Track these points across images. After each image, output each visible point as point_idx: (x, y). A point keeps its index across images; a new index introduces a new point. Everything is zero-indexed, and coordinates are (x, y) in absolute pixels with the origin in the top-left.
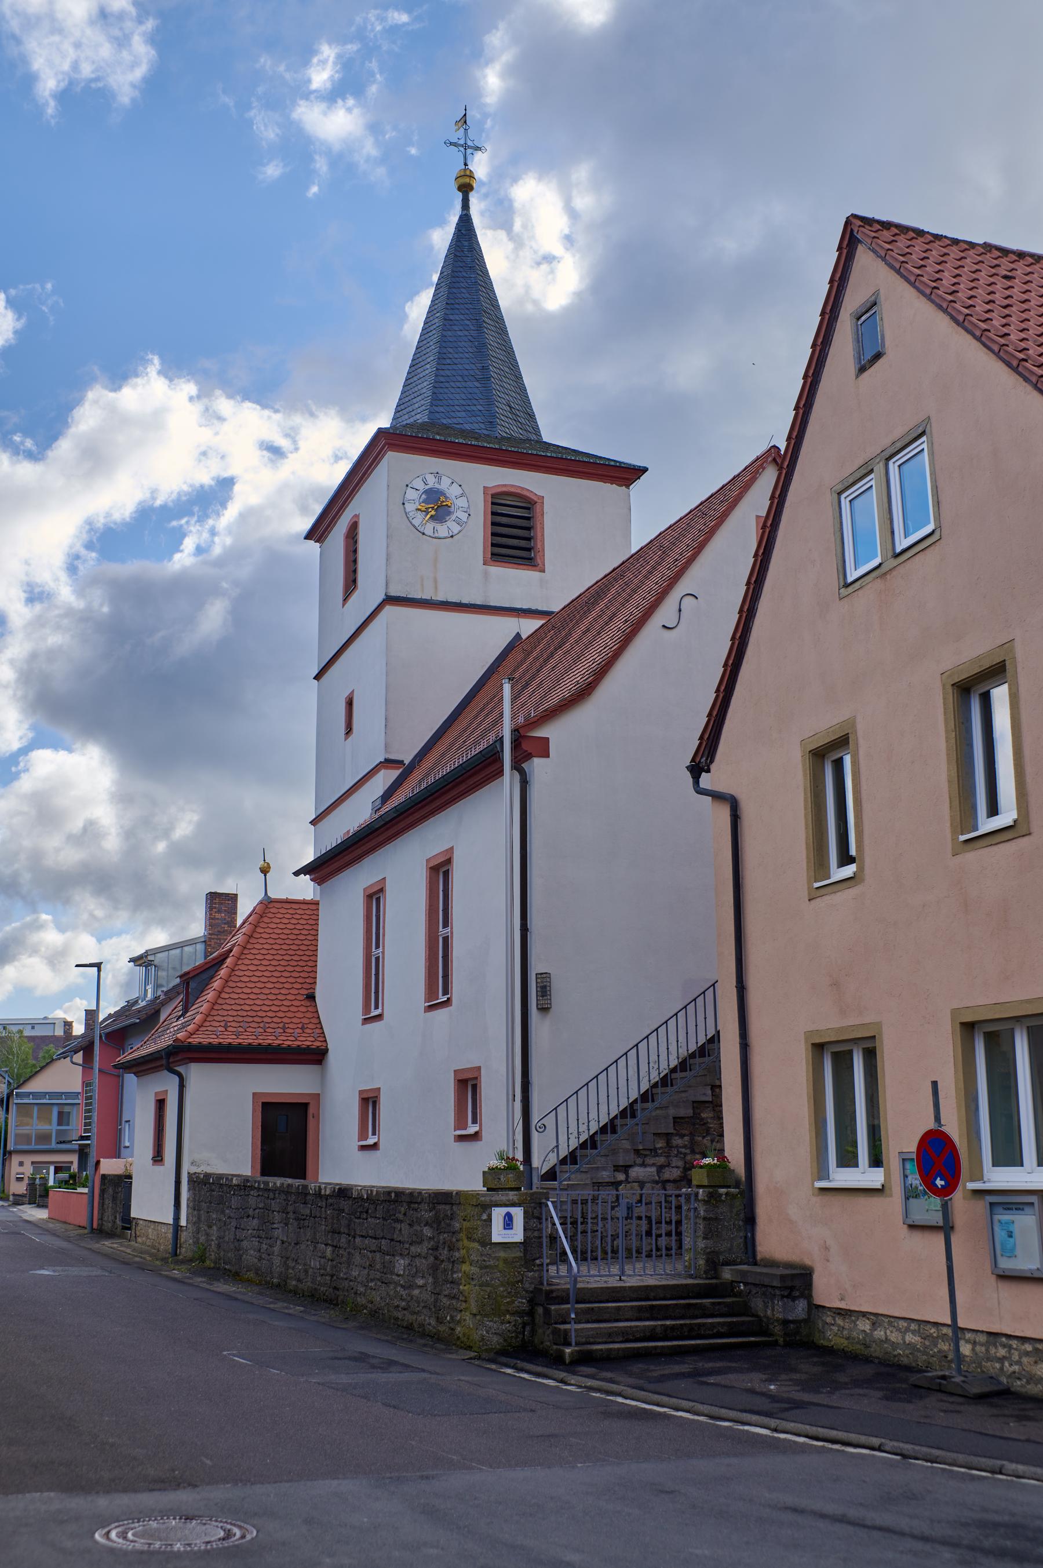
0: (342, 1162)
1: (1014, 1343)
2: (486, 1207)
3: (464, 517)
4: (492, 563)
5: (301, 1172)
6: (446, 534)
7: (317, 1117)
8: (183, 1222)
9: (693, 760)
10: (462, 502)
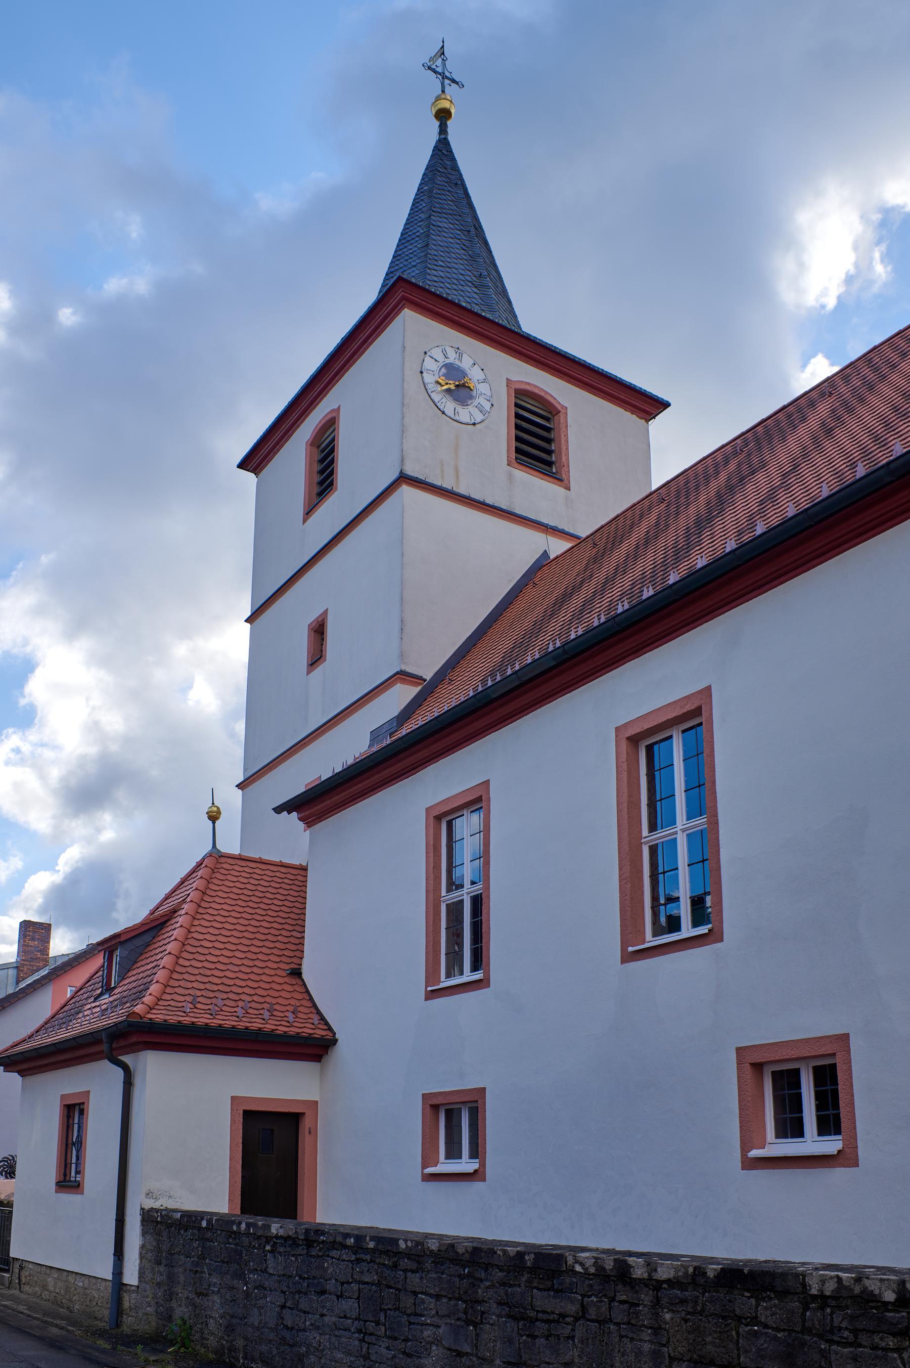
3: (487, 406)
4: (517, 465)
6: (468, 420)
7: (313, 1132)
10: (483, 388)
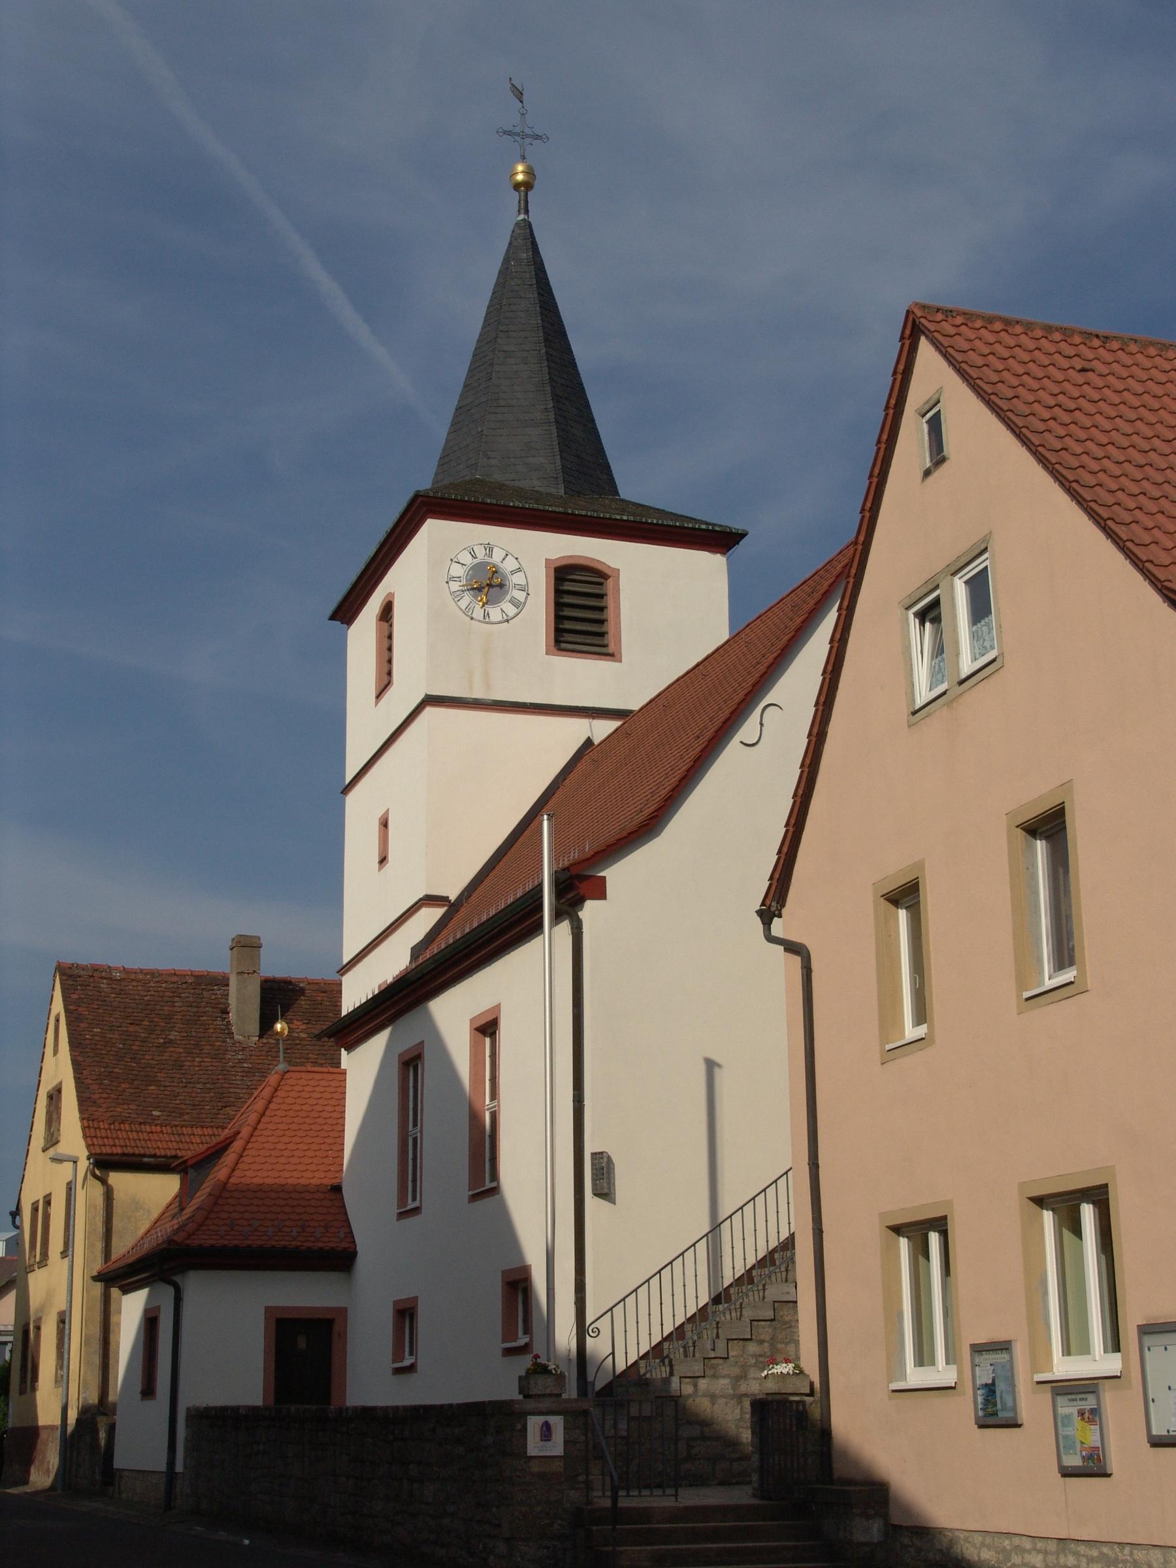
0: (369, 1379)
1: (1082, 1549)
2: (524, 1415)
3: (520, 596)
7: (343, 1335)
8: (179, 1468)
9: (763, 904)
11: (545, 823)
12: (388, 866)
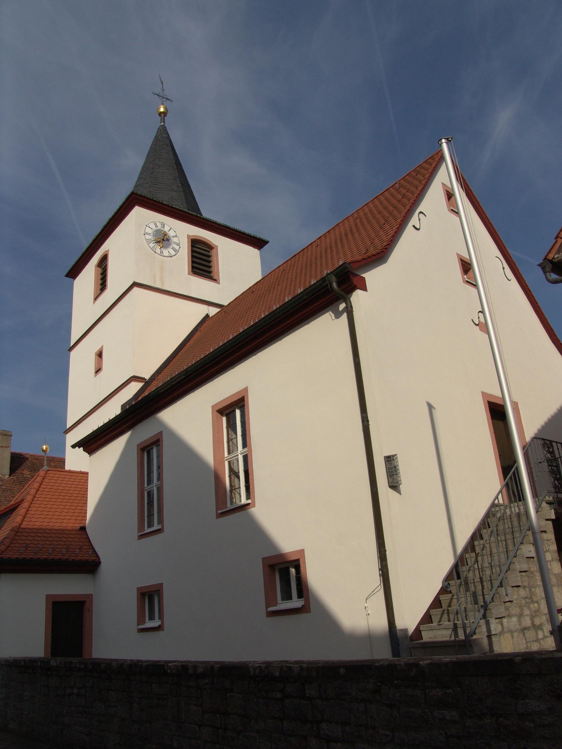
0: (115, 638)
3: (177, 247)
5: (80, 655)
6: (167, 255)
7: (90, 611)
11: (445, 146)
12: (101, 374)
